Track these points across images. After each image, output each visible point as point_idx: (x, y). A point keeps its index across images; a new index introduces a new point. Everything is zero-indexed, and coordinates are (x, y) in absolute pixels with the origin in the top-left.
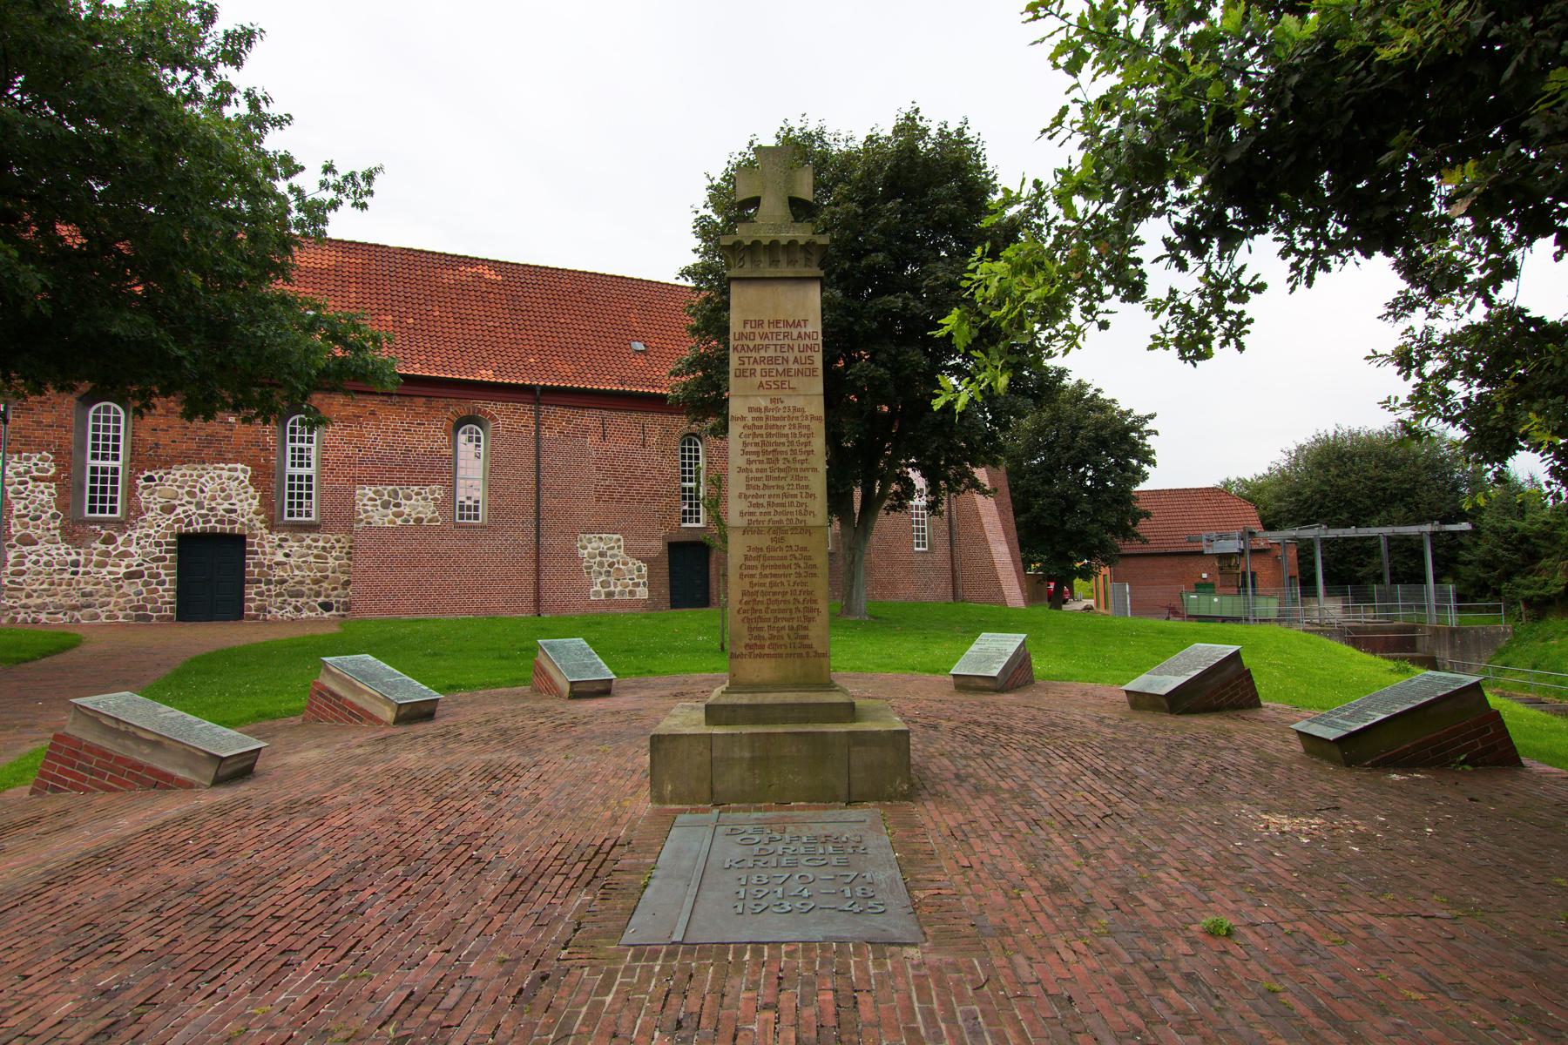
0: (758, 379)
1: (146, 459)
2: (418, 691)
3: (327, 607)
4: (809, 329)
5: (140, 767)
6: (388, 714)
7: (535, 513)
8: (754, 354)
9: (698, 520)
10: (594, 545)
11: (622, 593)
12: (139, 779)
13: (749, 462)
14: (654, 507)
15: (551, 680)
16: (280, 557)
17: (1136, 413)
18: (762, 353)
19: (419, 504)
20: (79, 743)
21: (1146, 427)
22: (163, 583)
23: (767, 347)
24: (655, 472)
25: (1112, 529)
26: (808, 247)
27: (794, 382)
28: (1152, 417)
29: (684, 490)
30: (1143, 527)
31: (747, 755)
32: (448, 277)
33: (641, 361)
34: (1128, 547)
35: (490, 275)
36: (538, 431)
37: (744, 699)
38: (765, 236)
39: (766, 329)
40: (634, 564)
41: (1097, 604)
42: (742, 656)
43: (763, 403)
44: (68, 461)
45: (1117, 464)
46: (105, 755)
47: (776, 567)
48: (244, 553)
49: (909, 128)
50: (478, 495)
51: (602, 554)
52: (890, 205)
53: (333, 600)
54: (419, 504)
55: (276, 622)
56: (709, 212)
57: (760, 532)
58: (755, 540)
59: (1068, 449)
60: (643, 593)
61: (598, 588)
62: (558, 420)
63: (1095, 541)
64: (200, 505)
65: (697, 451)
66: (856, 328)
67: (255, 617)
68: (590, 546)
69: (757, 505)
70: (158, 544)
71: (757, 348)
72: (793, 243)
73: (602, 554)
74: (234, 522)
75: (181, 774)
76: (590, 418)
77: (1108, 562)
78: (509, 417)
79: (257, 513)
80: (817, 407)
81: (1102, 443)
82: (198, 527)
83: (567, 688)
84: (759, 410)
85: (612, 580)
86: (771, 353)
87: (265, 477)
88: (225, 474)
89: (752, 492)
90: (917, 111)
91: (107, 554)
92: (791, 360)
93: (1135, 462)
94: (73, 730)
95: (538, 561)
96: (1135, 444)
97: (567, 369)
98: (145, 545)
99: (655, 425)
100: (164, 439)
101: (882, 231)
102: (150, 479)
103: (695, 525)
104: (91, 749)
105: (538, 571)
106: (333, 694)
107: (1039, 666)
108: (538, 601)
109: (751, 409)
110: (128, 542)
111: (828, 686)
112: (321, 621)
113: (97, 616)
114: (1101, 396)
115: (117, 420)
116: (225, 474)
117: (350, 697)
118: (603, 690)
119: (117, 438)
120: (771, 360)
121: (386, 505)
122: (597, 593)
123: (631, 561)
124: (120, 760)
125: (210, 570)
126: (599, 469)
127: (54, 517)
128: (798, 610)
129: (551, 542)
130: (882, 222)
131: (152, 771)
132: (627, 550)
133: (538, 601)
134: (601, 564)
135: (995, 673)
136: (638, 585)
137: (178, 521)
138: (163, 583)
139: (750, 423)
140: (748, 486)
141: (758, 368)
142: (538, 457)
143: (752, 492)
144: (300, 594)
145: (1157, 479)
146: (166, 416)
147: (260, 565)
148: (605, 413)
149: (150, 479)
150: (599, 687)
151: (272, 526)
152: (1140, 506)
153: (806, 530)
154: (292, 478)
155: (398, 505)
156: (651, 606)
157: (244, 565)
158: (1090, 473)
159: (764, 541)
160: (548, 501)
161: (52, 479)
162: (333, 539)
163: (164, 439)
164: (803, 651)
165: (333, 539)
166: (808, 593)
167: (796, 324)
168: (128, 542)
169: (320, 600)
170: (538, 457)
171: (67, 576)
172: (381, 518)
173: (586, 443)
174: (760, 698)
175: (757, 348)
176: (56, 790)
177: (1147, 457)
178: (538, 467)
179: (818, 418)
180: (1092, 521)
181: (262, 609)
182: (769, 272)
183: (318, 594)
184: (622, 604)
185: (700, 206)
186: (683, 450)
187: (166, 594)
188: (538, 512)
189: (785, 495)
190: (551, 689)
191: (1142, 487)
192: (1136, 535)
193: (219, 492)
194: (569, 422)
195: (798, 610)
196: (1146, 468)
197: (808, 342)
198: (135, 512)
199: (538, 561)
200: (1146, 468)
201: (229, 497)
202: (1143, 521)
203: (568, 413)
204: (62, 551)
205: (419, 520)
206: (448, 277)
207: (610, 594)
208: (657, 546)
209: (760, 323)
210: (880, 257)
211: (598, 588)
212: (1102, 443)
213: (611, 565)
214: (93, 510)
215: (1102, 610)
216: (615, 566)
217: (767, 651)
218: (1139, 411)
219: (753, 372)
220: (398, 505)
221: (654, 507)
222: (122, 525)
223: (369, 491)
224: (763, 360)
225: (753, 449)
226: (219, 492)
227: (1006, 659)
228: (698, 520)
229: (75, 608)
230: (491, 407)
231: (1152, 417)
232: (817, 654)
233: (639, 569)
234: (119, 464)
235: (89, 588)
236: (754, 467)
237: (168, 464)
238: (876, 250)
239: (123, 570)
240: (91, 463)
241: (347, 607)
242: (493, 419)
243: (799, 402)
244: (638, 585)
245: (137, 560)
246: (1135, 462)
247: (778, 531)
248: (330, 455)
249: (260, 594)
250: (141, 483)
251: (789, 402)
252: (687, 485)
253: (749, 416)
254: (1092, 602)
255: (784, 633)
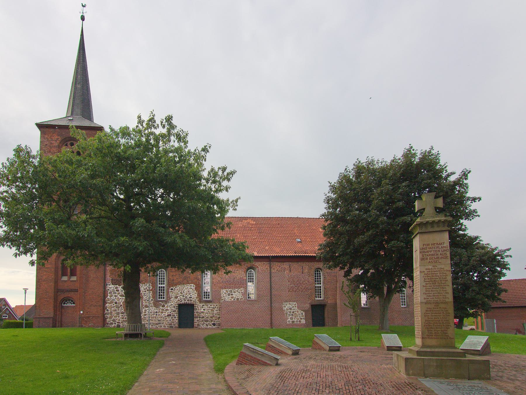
0: (428, 260)
1: (172, 284)
2: (295, 347)
3: (214, 324)
4: (445, 245)
5: (259, 360)
6: (290, 352)
7: (270, 296)
8: (427, 253)
9: (321, 297)
10: (288, 306)
11: (297, 321)
12: (260, 363)
13: (426, 284)
14: (306, 293)
15: (320, 345)
16: (202, 310)
17: (500, 249)
18: (430, 253)
19: (237, 294)
20: (245, 354)
21: (506, 254)
22: (175, 318)
23: (431, 251)
24: (306, 282)
25: (487, 297)
26: (444, 222)
27: (440, 261)
28: (508, 250)
29: (316, 287)
30: (503, 295)
31: (435, 364)
32: (240, 224)
33: (300, 245)
34: (494, 304)
35: (252, 222)
36: (270, 270)
37: (428, 350)
38: (430, 219)
39: (430, 246)
40: (300, 312)
41: (477, 328)
42: (426, 338)
43: (430, 267)
44: (154, 285)
45: (490, 270)
46: (252, 357)
47: (436, 313)
48: (194, 309)
49: (409, 154)
50: (209, 290)
51: (290, 309)
52: (404, 184)
53: (216, 323)
54: (237, 294)
55: (202, 329)
56: (330, 194)
57: (430, 303)
58: (429, 306)
59: (466, 265)
60: (303, 321)
61: (289, 320)
62: (276, 266)
63: (480, 302)
64: (183, 296)
65: (320, 274)
66: (391, 229)
67: (197, 327)
68: (287, 306)
69: (429, 296)
70: (174, 307)
71: (428, 252)
72: (440, 221)
73: (290, 309)
74: (191, 301)
75: (268, 362)
76: (286, 265)
77: (486, 311)
78: (262, 266)
79: (197, 298)
80: (448, 267)
81: (483, 262)
82: (183, 302)
83: (328, 348)
84: (429, 269)
85: (294, 317)
86: (432, 253)
87: (199, 287)
88: (189, 287)
89: (427, 292)
90: (411, 147)
91: (163, 310)
92: (439, 254)
93: (499, 269)
94: (243, 351)
95: (271, 311)
96: (499, 261)
97: (278, 250)
98: (171, 307)
99: (306, 266)
100: (175, 278)
101: (401, 194)
102: (172, 289)
103: (319, 299)
104: (248, 355)
105: (271, 314)
106: (273, 346)
107: (492, 349)
108: (271, 323)
109: (426, 269)
110: (167, 307)
111: (454, 347)
112: (212, 329)
113: (161, 326)
114: (481, 242)
115: (164, 274)
116: (189, 287)
117: (278, 347)
118: (338, 349)
119: (164, 279)
120: (432, 255)
121: (229, 295)
122: (289, 321)
123: (299, 311)
124: (255, 358)
125: (186, 313)
126: (289, 281)
127: (152, 300)
128: (444, 325)
129: (275, 305)
130: (400, 190)
131: (262, 361)
132: (298, 307)
133: (271, 323)
134: (290, 312)
135: (479, 349)
136: (302, 319)
137: (179, 300)
138: (175, 318)
139: (426, 273)
140: (426, 291)
141: (428, 257)
142: (271, 278)
143: (427, 292)
144: (207, 321)
145: (509, 275)
146: (174, 273)
147: (197, 312)
148: (290, 263)
149: (172, 289)
150: (337, 348)
151: (201, 301)
152: (502, 287)
153: (446, 303)
154: (159, 287)
155: (232, 295)
156: (306, 325)
157: (193, 313)
158: (475, 275)
159: (432, 306)
160: (273, 293)
161: (151, 290)
162: (215, 305)
163: (175, 278)
164: (446, 337)
165: (215, 305)
166: (447, 321)
167: (441, 244)
168: (167, 307)
169: (213, 322)
170: (271, 278)
171: (155, 316)
172: (228, 298)
173: (284, 274)
174: (433, 350)
175: (428, 252)
176: (241, 364)
177: (504, 266)
178: (271, 280)
179: (449, 271)
180: (478, 293)
181: (198, 325)
182: (431, 230)
183: (212, 321)
184: (296, 325)
185: (327, 192)
186: (315, 274)
187: (176, 320)
188: (271, 295)
189: (438, 293)
190: (321, 348)
191: (503, 279)
192: (499, 299)
193: (186, 292)
194: (279, 267)
195: (444, 325)
196: (504, 271)
197: (445, 249)
198: (169, 298)
199: (271, 311)
200: (504, 271)
201: (190, 294)
202: (503, 294)
203: (279, 264)
204: (153, 309)
205: (238, 299)
206: (240, 224)
207: (293, 322)
208: (308, 306)
209: (428, 245)
210: (401, 203)
211: (289, 320)
212: (483, 262)
213: (293, 312)
214: (159, 298)
215: (480, 330)
216: (294, 312)
217: (434, 337)
218: (501, 247)
219: (427, 259)
220: (232, 295)
221: (306, 293)
222: (166, 302)
223: (224, 291)
224: (430, 255)
225: (428, 280)
226: (186, 292)
227: (483, 344)
228: (321, 297)
229: (157, 324)
230: (257, 264)
231: (508, 250)
232: (450, 338)
233: (302, 314)
234: (164, 285)
235: (160, 319)
236: (428, 285)
237: (176, 285)
238: (399, 201)
239: (167, 314)
240: (159, 285)
241: (219, 325)
242: (258, 267)
243: (443, 266)
244: (302, 319)
245: (170, 311)
246: (499, 269)
247: (437, 303)
248: (214, 281)
249: (198, 321)
250: (170, 290)
251: (440, 267)
252: (317, 285)
253: (426, 271)
254: (474, 327)
255: (439, 332)
